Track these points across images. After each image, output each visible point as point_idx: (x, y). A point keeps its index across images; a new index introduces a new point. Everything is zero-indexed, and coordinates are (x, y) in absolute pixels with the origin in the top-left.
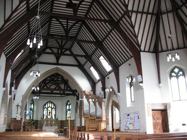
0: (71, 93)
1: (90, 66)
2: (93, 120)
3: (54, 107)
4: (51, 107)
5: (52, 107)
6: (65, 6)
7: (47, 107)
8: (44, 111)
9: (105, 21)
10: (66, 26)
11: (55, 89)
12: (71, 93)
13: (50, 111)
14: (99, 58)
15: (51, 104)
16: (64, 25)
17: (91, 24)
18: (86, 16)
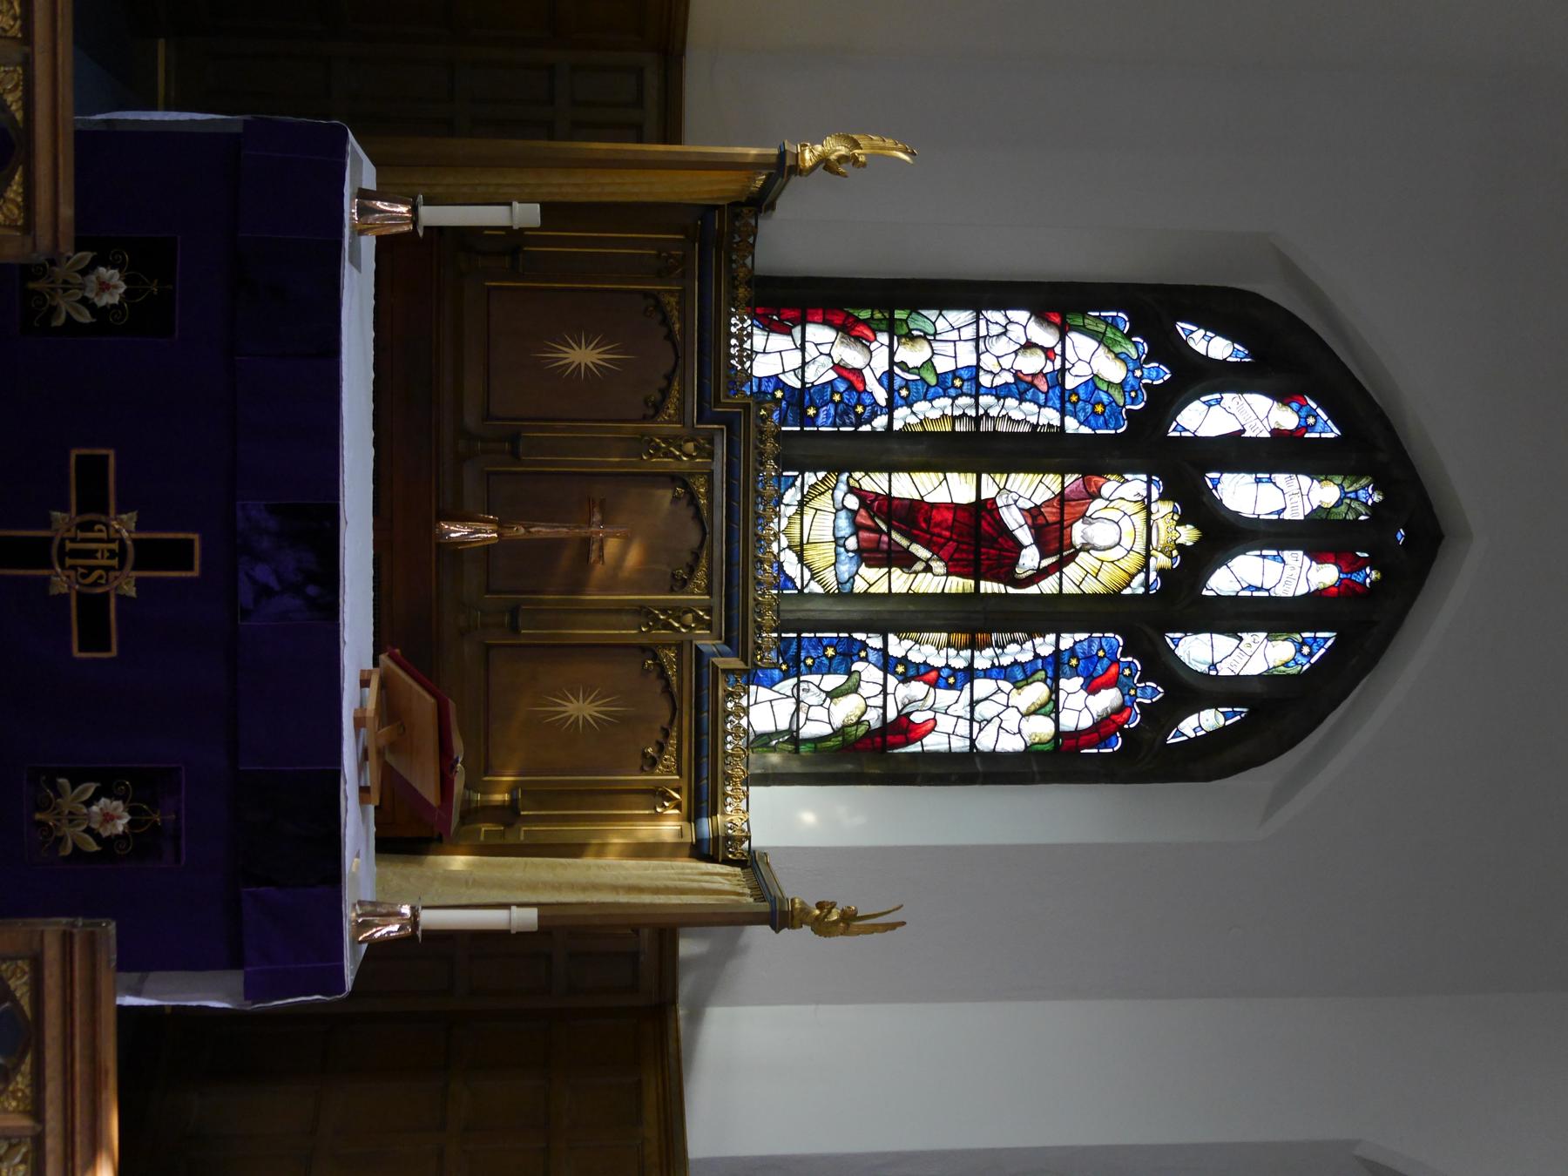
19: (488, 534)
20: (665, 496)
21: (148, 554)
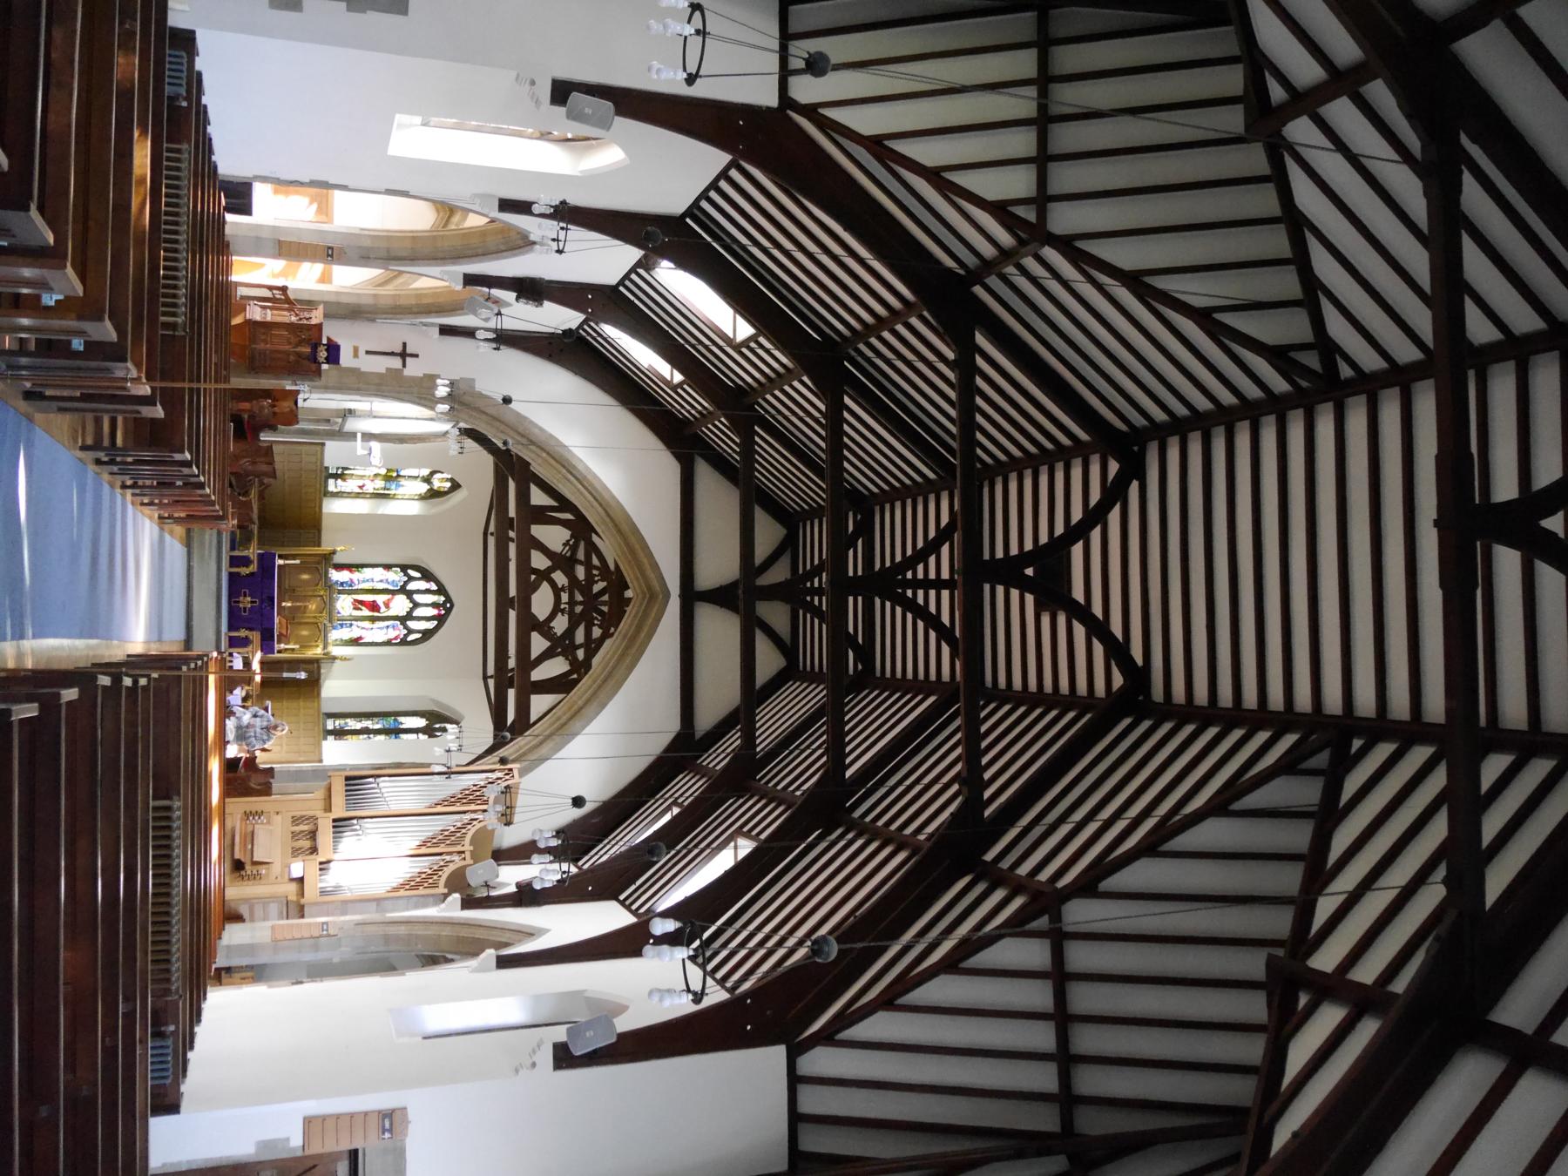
2: (307, 844)
3: (412, 637)
5: (412, 624)
7: (412, 586)
8: (388, 567)
10: (920, 575)
13: (387, 605)
15: (434, 612)
19: (289, 605)
20: (319, 598)
21: (252, 602)
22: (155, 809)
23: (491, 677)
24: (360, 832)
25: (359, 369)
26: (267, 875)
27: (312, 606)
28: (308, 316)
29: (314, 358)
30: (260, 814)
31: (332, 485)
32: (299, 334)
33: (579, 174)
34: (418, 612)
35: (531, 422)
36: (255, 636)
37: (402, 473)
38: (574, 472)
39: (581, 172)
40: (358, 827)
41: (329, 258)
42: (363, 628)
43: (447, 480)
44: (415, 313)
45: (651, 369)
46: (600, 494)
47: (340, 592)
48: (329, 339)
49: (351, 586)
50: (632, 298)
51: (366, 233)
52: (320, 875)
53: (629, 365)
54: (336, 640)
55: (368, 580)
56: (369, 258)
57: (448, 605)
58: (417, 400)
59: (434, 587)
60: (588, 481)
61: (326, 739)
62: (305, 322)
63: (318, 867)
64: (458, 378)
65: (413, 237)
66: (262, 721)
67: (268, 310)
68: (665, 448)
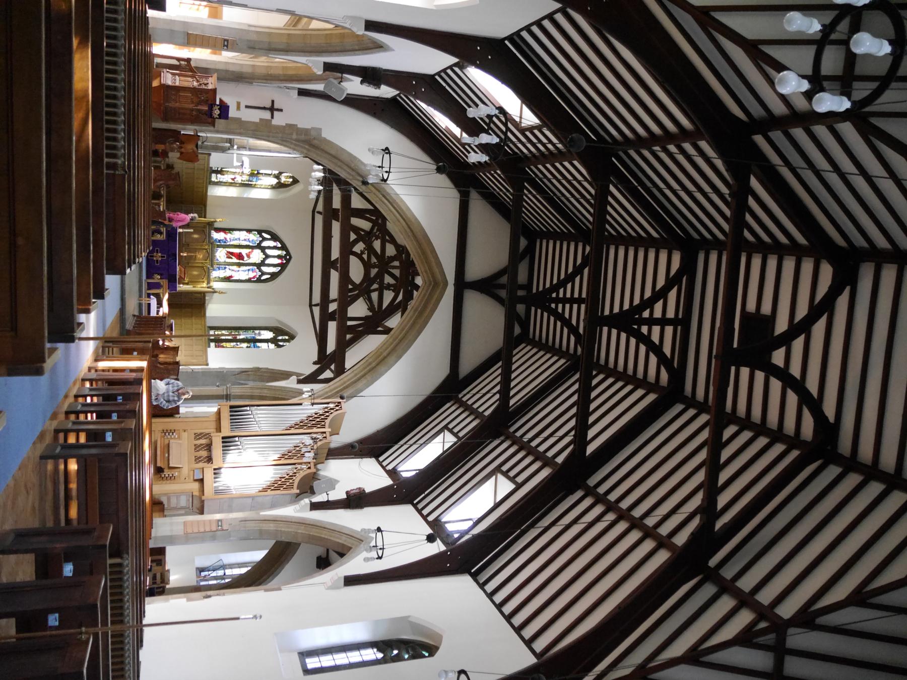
0: (331, 346)
1: (455, 430)
2: (204, 453)
3: (264, 277)
4: (268, 261)
5: (264, 269)
6: (751, 306)
7: (265, 244)
8: (249, 231)
9: (709, 511)
10: (561, 295)
11: (345, 278)
12: (331, 346)
13: (248, 256)
14: (500, 476)
15: (277, 261)
16: (561, 291)
17: (570, 389)
18: (732, 418)
19: (185, 255)
20: (205, 251)
21: (162, 257)
22: (111, 565)
23: (316, 305)
24: (240, 447)
25: (241, 119)
26: (179, 476)
27: (200, 256)
28: (206, 82)
29: (210, 114)
30: (172, 432)
31: (214, 178)
32: (199, 96)
33: (434, 8)
34: (268, 261)
35: (359, 160)
36: (164, 283)
37: (261, 172)
38: (388, 197)
39: (435, 6)
40: (239, 443)
41: (225, 48)
42: (233, 270)
43: (291, 177)
44: (281, 80)
45: (447, 129)
46: (404, 213)
47: (219, 246)
48: (221, 100)
49: (225, 242)
50: (444, 84)
51: (253, 29)
52: (215, 478)
53: (428, 121)
54: (215, 277)
55: (236, 239)
56: (254, 48)
57: (288, 257)
58: (280, 142)
59: (279, 245)
60: (397, 203)
61: (209, 347)
62: (204, 87)
63: (213, 472)
64: (310, 127)
65: (289, 35)
66: (173, 387)
67: (177, 77)
68: (451, 185)
